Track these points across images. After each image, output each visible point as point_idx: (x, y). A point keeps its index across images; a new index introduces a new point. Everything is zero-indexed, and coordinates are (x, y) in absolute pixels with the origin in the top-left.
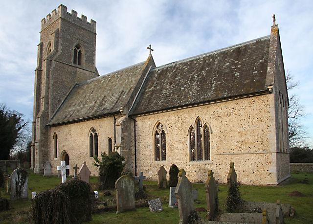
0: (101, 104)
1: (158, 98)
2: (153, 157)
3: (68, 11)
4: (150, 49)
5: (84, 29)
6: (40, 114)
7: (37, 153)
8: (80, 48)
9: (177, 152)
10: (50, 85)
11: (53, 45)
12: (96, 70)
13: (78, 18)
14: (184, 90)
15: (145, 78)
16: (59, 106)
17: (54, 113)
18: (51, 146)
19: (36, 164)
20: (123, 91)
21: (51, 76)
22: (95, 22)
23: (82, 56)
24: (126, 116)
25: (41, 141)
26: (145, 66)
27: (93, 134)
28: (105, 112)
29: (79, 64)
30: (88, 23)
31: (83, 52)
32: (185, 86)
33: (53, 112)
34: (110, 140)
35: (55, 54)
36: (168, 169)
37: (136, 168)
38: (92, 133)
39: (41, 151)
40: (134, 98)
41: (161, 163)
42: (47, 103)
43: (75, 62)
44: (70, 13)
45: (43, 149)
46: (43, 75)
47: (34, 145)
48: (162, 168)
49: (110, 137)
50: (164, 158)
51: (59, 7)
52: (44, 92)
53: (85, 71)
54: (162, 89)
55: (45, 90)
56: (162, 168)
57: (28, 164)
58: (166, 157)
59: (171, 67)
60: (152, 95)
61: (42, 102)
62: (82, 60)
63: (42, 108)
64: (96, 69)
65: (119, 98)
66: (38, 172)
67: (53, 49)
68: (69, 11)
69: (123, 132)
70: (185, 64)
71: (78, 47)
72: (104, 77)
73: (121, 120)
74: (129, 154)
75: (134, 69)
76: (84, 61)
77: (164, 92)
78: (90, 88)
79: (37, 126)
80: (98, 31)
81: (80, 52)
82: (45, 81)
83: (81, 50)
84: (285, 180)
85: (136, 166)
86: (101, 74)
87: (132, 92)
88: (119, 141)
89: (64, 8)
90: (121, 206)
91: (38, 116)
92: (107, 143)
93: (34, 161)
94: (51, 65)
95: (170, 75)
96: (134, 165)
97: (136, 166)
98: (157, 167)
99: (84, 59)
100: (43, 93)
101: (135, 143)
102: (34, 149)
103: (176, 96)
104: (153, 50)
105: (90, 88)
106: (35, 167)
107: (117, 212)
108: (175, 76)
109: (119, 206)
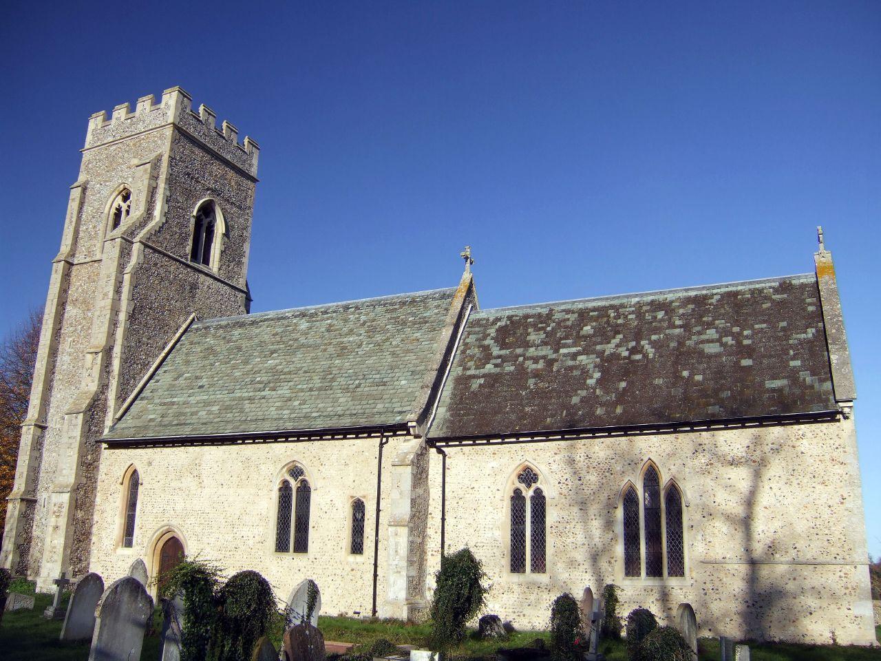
2: (506, 562)
33: (124, 400)
43: (195, 256)
49: (358, 495)
50: (539, 565)
71: (207, 210)
101: (443, 519)
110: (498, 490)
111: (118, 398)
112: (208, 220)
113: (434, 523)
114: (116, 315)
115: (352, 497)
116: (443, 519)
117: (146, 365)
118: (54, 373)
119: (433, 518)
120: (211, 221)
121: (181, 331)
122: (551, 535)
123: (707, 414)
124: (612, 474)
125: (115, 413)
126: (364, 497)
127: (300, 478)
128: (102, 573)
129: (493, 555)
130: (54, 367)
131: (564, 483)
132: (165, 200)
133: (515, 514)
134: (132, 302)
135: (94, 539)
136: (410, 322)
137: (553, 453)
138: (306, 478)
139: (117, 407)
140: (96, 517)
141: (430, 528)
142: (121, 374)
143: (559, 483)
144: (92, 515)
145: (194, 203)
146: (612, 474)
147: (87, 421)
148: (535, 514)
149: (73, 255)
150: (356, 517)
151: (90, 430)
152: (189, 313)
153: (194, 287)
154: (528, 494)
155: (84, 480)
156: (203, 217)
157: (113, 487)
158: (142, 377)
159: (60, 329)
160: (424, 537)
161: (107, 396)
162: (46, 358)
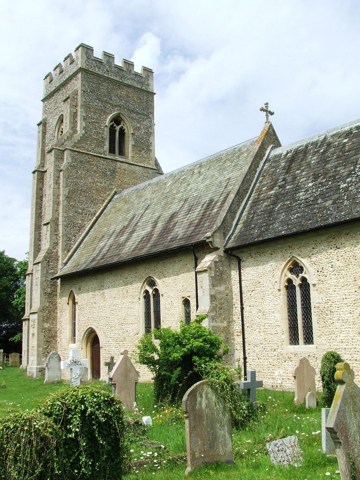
0: (167, 230)
1: (289, 210)
2: (286, 336)
3: (135, 70)
4: (266, 111)
5: (129, 86)
6: (41, 256)
7: (33, 335)
8: (122, 122)
9: (337, 325)
10: (61, 198)
11: (67, 121)
12: (157, 164)
13: (117, 67)
14: (346, 189)
15: (259, 170)
16: (81, 238)
17: (70, 253)
18: (63, 319)
19: (31, 358)
20: (211, 201)
21: (61, 181)
22: (272, 115)
23: (126, 139)
24: (221, 252)
25: (43, 309)
26: (257, 147)
27: (150, 291)
28: (175, 245)
29: (122, 153)
30: (136, 75)
31: (129, 130)
32: (349, 179)
33: (69, 251)
34: (186, 302)
35: (70, 138)
36: (317, 365)
37: (245, 363)
38: (148, 288)
39: (42, 329)
40: (235, 213)
41: (302, 348)
42: (55, 232)
43: (112, 150)
44: (121, 65)
45: (46, 325)
46: (48, 179)
47: (29, 320)
48: (304, 362)
49: (186, 296)
50: (309, 340)
51: (77, 49)
52: (50, 213)
53: (133, 167)
54: (297, 189)
55: (51, 208)
56: (304, 362)
57: (17, 359)
58: (314, 336)
59: (315, 144)
60: (274, 203)
61: (46, 231)
62: (126, 146)
63: (46, 245)
64: (156, 161)
65: (204, 215)
66: (35, 376)
67: (66, 127)
68: (98, 54)
69: (213, 285)
70: (348, 134)
71: (117, 120)
72: (171, 175)
73: (208, 260)
74: (227, 331)
75: (233, 153)
76: (130, 146)
77: (301, 195)
78: (143, 199)
79: (34, 281)
80: (156, 87)
81: (122, 132)
82: (52, 190)
83: (125, 127)
84: (186, 405)
85: (245, 358)
86: (166, 169)
87: (231, 201)
88: (205, 305)
89: (87, 50)
90: (197, 455)
91: (37, 261)
92: (180, 308)
93: (28, 350)
94: (62, 159)
95: (313, 160)
96: (242, 356)
97: (245, 358)
98: (294, 358)
99: (130, 143)
100: (48, 216)
101: (242, 309)
102: (28, 327)
103: (330, 202)
104: (272, 114)
105: (143, 199)
106: (30, 362)
107: (189, 469)
108: (323, 160)
109: (193, 454)
110: (276, 282)
111: (63, 250)
112: (120, 126)
113: (236, 311)
114: (57, 198)
115: (183, 298)
116: (242, 309)
117: (82, 227)
118: (40, 241)
119: (236, 307)
120: (122, 127)
121: (106, 201)
122: (315, 314)
123: (332, 467)
124: (356, 259)
125: (63, 260)
126: (189, 297)
127: (154, 287)
128: (163, 321)
129: (276, 332)
130: (40, 236)
131: (321, 272)
132: (82, 119)
133: (290, 299)
134: (67, 189)
135: (58, 339)
136: (343, 188)
137: (311, 248)
138: (157, 287)
139: (64, 256)
140: (58, 327)
141: (235, 315)
142: (65, 235)
143: (318, 271)
144: (56, 325)
145: (106, 117)
146: (356, 259)
147: (45, 267)
148: (304, 298)
149: (43, 166)
150: (187, 312)
151: (47, 272)
152: (112, 190)
153: (114, 172)
154: (297, 282)
155: (48, 304)
156: (115, 125)
157: (64, 307)
158: (80, 235)
159: (41, 213)
160: (229, 322)
161: (57, 250)
162: (34, 232)
